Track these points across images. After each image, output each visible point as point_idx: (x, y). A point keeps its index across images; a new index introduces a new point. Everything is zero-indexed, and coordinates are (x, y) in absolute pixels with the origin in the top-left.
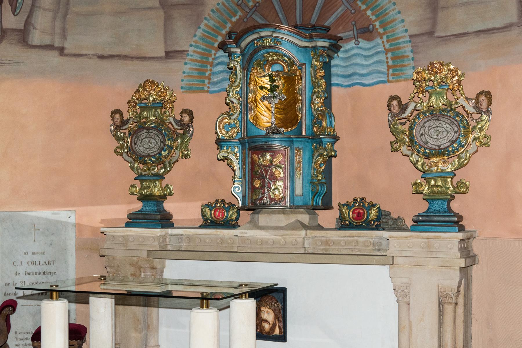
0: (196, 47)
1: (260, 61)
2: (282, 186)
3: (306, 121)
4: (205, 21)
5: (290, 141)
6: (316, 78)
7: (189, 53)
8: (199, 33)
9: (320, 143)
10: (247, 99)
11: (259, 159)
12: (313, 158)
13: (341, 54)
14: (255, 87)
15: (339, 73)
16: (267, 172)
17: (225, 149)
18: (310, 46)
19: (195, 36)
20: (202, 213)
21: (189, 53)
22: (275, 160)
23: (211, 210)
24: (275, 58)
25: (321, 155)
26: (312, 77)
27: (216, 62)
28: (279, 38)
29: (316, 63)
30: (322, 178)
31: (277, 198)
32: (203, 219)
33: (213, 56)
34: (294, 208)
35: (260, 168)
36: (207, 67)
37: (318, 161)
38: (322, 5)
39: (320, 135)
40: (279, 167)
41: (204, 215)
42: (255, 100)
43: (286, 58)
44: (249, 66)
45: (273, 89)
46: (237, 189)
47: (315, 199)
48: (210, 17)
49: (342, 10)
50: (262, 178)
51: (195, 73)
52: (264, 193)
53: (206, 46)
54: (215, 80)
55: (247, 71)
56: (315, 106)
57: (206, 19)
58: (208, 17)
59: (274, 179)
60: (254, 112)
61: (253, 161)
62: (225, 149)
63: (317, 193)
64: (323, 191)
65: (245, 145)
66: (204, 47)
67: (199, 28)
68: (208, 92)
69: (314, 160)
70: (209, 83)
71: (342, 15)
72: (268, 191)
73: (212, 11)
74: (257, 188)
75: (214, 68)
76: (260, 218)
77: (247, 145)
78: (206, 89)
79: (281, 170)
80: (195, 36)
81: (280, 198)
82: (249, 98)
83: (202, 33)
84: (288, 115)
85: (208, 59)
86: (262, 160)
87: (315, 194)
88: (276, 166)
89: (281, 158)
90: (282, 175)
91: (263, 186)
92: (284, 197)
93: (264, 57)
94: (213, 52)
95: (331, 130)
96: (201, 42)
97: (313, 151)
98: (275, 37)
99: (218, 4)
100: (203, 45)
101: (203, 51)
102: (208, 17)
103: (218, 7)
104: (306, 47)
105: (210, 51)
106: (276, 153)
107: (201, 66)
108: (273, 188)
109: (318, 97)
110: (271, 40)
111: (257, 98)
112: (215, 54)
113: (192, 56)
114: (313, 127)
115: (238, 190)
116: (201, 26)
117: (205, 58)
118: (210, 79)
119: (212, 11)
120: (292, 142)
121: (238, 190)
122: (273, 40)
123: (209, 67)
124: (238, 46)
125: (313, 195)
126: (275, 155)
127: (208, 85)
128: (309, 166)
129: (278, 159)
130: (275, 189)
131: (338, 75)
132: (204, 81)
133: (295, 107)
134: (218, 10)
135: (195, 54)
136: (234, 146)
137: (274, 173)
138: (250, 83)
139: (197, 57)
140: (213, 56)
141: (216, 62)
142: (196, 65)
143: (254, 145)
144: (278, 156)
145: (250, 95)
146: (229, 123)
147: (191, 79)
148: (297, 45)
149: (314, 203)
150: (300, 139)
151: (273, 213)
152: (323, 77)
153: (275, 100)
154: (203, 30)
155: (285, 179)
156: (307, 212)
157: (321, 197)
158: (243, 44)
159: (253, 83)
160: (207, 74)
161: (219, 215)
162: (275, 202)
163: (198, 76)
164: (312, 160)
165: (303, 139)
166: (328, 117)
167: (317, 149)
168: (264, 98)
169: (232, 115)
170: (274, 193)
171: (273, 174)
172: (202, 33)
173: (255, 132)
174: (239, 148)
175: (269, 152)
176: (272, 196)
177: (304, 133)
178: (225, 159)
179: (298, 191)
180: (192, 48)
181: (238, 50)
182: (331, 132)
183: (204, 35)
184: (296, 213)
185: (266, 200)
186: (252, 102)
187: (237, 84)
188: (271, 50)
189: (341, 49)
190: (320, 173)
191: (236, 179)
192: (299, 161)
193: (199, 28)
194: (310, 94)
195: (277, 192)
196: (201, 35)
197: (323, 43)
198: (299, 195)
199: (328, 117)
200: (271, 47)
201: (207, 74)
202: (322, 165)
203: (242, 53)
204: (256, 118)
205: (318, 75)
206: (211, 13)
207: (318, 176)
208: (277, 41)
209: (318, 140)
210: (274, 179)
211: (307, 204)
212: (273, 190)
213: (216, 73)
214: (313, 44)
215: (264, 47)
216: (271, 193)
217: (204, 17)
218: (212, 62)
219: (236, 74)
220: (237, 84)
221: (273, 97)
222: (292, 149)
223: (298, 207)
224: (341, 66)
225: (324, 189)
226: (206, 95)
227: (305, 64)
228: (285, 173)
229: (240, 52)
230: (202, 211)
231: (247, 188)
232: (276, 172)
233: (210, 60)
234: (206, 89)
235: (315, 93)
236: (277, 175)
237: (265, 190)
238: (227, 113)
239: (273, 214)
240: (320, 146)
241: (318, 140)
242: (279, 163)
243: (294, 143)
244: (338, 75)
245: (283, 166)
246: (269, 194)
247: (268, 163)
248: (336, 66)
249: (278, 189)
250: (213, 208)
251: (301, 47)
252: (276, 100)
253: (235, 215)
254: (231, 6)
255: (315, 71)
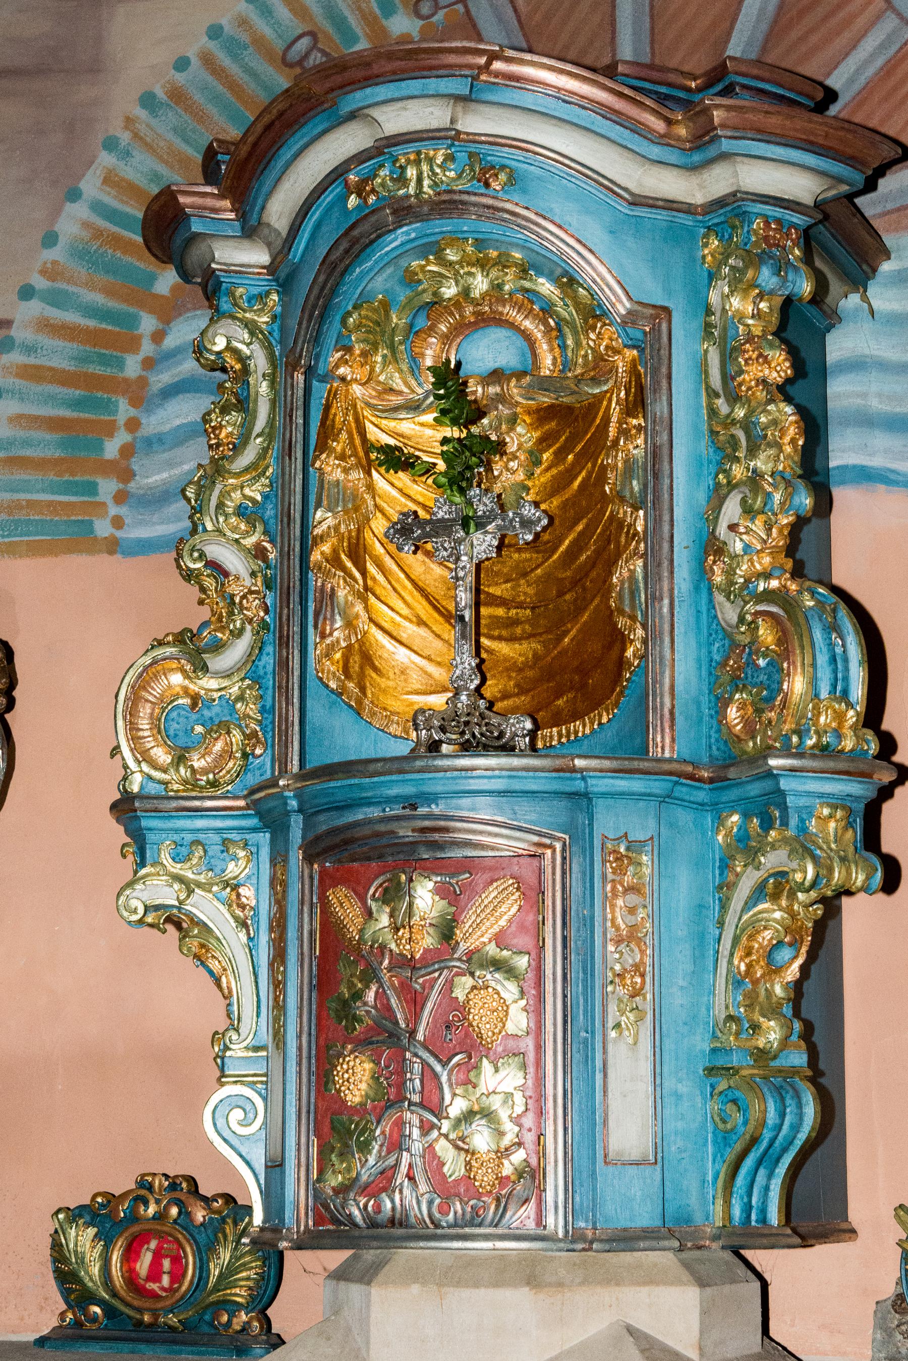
0: (56, 299)
1: (386, 306)
2: (519, 1098)
3: (681, 666)
4: (106, 159)
5: (572, 795)
6: (734, 398)
7: (13, 332)
8: (73, 221)
9: (770, 808)
10: (307, 543)
11: (369, 914)
12: (724, 906)
13: (882, 297)
14: (357, 475)
15: (876, 405)
16: (416, 1002)
17: (166, 858)
18: (699, 198)
19: (50, 239)
20: (55, 1260)
21: (13, 332)
22: (469, 919)
23: (106, 1238)
24: (480, 284)
25: (777, 887)
26: (712, 394)
27: (162, 378)
28: (496, 141)
29: (736, 302)
30: (785, 1042)
31: (484, 1178)
32: (66, 1294)
33: (147, 348)
34: (602, 1242)
35: (370, 975)
36: (108, 407)
37: (753, 929)
38: (764, 27)
39: (767, 751)
40: (497, 965)
41: (66, 1276)
42: (357, 551)
43: (546, 287)
44: (316, 339)
45: (469, 462)
46: (238, 1114)
47: (741, 1180)
48: (136, 136)
49: (882, 47)
50: (386, 1039)
51: (46, 446)
52: (397, 1144)
53: (109, 291)
54: (156, 479)
55: (310, 372)
56: (730, 573)
57: (110, 144)
58: (125, 137)
59: (464, 1045)
60: (349, 624)
61: (331, 934)
62: (166, 858)
63: (754, 1141)
64: (796, 1128)
65: (286, 828)
66: (99, 299)
67: (74, 195)
68: (113, 546)
69: (731, 919)
70: (121, 498)
71: (888, 70)
72: (426, 1128)
73: (148, 101)
74: (354, 1110)
75: (149, 412)
76: (376, 1313)
77: (296, 824)
78: (103, 528)
79: (509, 990)
80: (50, 239)
81: (503, 1181)
82: (322, 538)
83: (86, 225)
84: (566, 656)
85: (121, 365)
86: (384, 920)
87: (741, 1153)
88: (476, 961)
89: (510, 909)
90: (518, 1020)
91: (390, 1096)
92: (532, 1174)
93: (410, 279)
94: (148, 323)
95: (840, 717)
96: (81, 271)
97: (725, 865)
98: (473, 139)
99: (182, 64)
100: (90, 286)
101: (91, 323)
102: (125, 137)
103: (180, 78)
104: (670, 205)
105: (132, 321)
106: (481, 878)
107: (77, 404)
108: (457, 1107)
109: (748, 511)
110: (450, 158)
111: (368, 535)
112: (158, 337)
113: (30, 349)
114: (723, 703)
115: (240, 1123)
116: (83, 185)
117: (104, 361)
118: (127, 475)
119: (148, 101)
120: (581, 800)
121: (240, 1123)
122: (462, 157)
123: (124, 410)
124: (251, 229)
125: (730, 1154)
126: (471, 891)
127: (113, 510)
128: (698, 957)
129: (493, 916)
130: (468, 1116)
131: (867, 421)
132: (92, 489)
133: (604, 586)
134: (177, 96)
135: (47, 341)
136: (226, 844)
137: (463, 1009)
138: (322, 446)
139: (59, 355)
140: (147, 348)
141: (162, 378)
142: (50, 399)
143: (345, 837)
144: (492, 892)
145: (324, 519)
146: (195, 699)
147: (22, 476)
148: (611, 188)
149: (737, 1212)
150: (636, 784)
151: (466, 1274)
152: (784, 391)
153: (477, 537)
154: (97, 207)
155: (539, 1048)
156: (686, 1265)
157: (782, 1170)
158: (279, 209)
159: (338, 446)
160: (111, 449)
161: (155, 1274)
162: (472, 1206)
163: (56, 463)
164: (721, 924)
165: (657, 785)
166: (818, 634)
167: (747, 848)
168: (409, 530)
169: (218, 647)
170: (461, 1145)
171: (455, 1017)
172: (86, 225)
173: (344, 737)
174: (253, 856)
175: (430, 868)
176: (454, 1166)
177: (663, 745)
178: (176, 921)
179: (629, 1128)
180: (34, 308)
181: (256, 256)
182: (839, 736)
183: (98, 233)
184: (613, 1280)
185: (411, 1198)
186: (334, 560)
187: (248, 457)
188: (442, 226)
189: (886, 267)
190: (772, 1011)
191: (237, 1051)
192: (633, 928)
193: (74, 195)
194: (702, 497)
195: (481, 1139)
196: (86, 234)
197: (784, 177)
198: (635, 1155)
199: (818, 634)
200: (447, 205)
201: (111, 449)
202: (785, 954)
203: (281, 274)
204: (361, 661)
205: (753, 372)
206: (141, 113)
207: (755, 1027)
208: (485, 164)
209: (755, 789)
210: (464, 1045)
211: (688, 1220)
212: (458, 1122)
213: (160, 439)
214: (717, 182)
215: (404, 212)
216: (443, 1148)
217: (101, 137)
218: (142, 382)
219: (243, 404)
220: (248, 457)
221: (465, 523)
222: (579, 838)
223: (625, 1240)
224: (883, 366)
225: (800, 1116)
226: (103, 563)
227: (667, 310)
228: (537, 1010)
229: (271, 269)
230: (57, 1249)
231: (292, 1111)
232: (476, 1000)
233: (132, 367)
234: (103, 528)
235: (732, 486)
236: (481, 1018)
237: (400, 1124)
238: (183, 638)
239: (459, 1284)
240: (767, 824)
241: (755, 789)
242: (499, 939)
243: (600, 806)
244: (867, 421)
245: (522, 962)
246: (430, 1148)
247: (428, 941)
248: (856, 365)
249: (488, 1115)
250: (120, 1225)
251: (638, 201)
252: (483, 543)
253: (249, 1274)
254: (253, 73)
255: (729, 355)
